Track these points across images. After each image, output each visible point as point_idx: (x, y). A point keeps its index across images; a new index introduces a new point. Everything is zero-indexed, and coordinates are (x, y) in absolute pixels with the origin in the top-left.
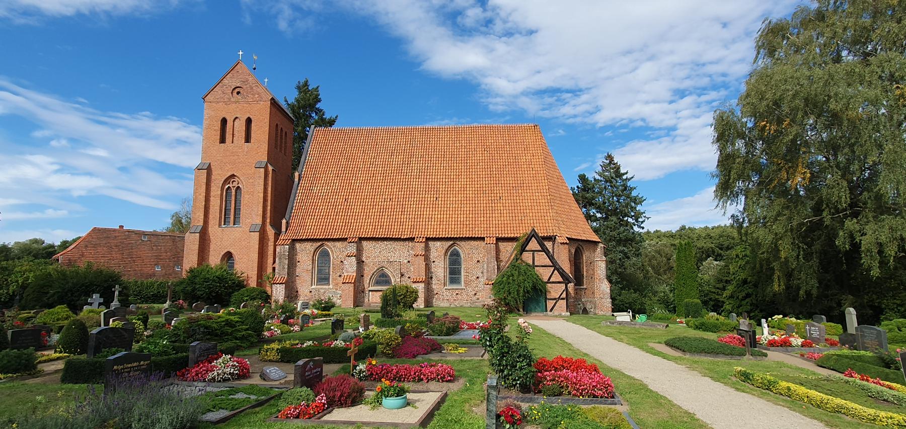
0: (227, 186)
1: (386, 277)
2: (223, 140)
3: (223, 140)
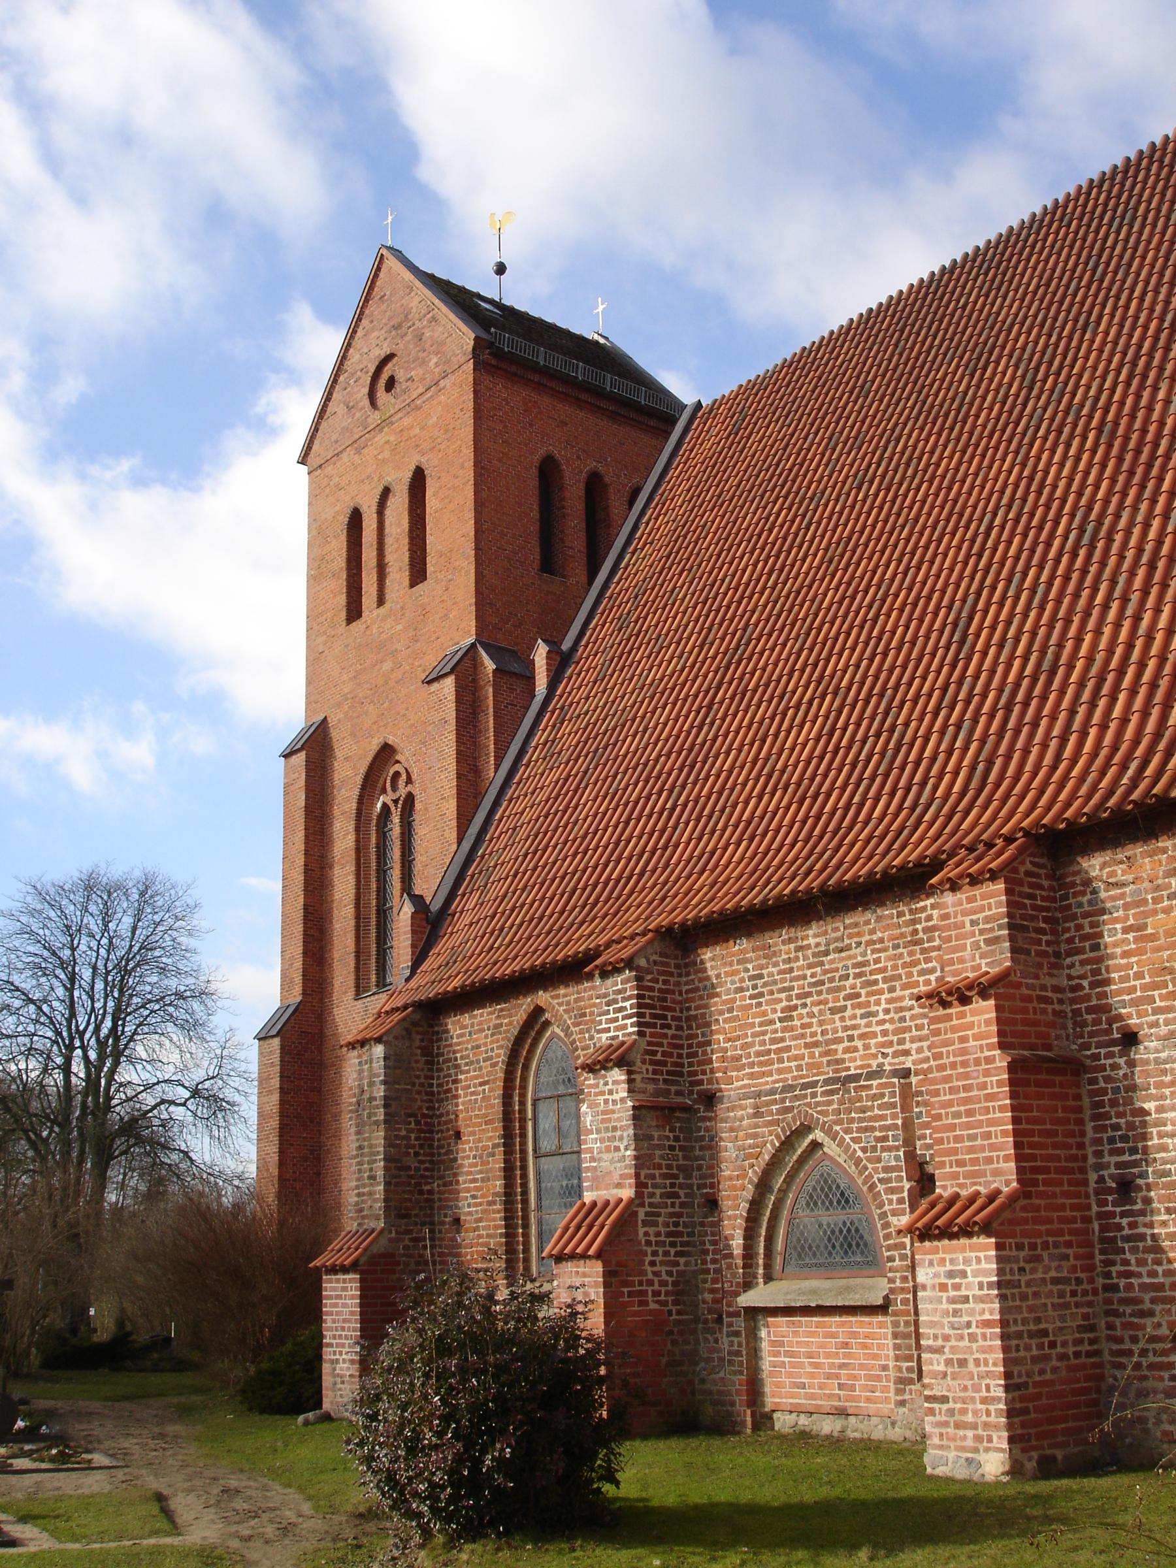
0: (379, 805)
1: (844, 1200)
2: (354, 612)
3: (354, 612)
